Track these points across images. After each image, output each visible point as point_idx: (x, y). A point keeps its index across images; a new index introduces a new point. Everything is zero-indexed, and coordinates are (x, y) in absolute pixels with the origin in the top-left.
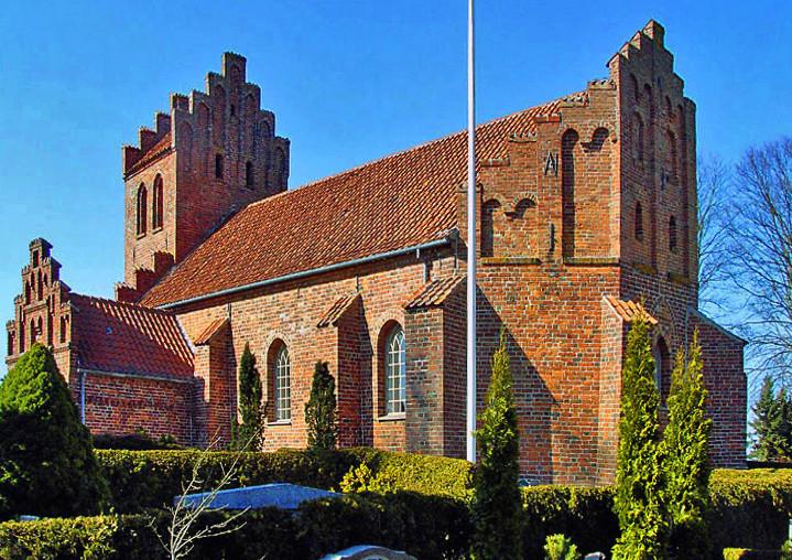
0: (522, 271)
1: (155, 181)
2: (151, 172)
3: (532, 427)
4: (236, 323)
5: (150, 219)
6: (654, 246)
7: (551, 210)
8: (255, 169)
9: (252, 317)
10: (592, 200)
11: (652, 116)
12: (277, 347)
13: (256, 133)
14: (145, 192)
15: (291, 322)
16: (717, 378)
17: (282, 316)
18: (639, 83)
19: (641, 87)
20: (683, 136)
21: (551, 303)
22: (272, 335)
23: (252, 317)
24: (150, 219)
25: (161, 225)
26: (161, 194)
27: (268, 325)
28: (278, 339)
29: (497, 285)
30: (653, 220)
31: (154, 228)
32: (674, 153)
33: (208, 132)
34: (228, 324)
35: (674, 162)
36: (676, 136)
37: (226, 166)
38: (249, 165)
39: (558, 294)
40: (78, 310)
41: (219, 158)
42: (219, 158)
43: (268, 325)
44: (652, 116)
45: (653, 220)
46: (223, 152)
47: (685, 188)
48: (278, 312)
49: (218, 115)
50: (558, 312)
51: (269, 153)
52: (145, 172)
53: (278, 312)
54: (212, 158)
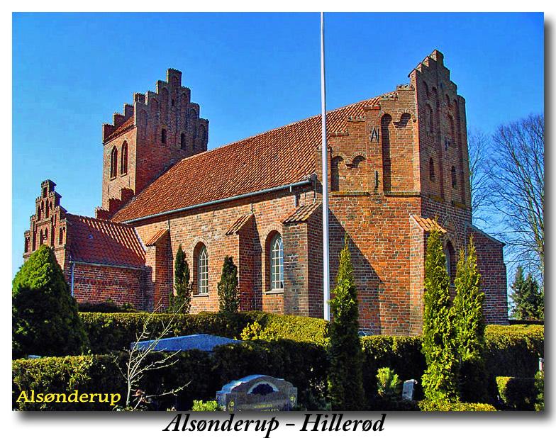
4: (173, 233)
8: (187, 137)
9: (184, 229)
12: (200, 247)
14: (116, 151)
15: (209, 231)
16: (487, 267)
20: (458, 118)
21: (377, 219)
22: (197, 240)
23: (184, 229)
26: (126, 153)
28: (200, 242)
29: (342, 209)
32: (452, 128)
33: (157, 116)
34: (168, 233)
35: (453, 133)
36: (454, 118)
38: (183, 135)
39: (381, 214)
41: (164, 131)
42: (164, 131)
45: (441, 169)
46: (166, 128)
49: (163, 106)
52: (117, 140)
54: (159, 131)
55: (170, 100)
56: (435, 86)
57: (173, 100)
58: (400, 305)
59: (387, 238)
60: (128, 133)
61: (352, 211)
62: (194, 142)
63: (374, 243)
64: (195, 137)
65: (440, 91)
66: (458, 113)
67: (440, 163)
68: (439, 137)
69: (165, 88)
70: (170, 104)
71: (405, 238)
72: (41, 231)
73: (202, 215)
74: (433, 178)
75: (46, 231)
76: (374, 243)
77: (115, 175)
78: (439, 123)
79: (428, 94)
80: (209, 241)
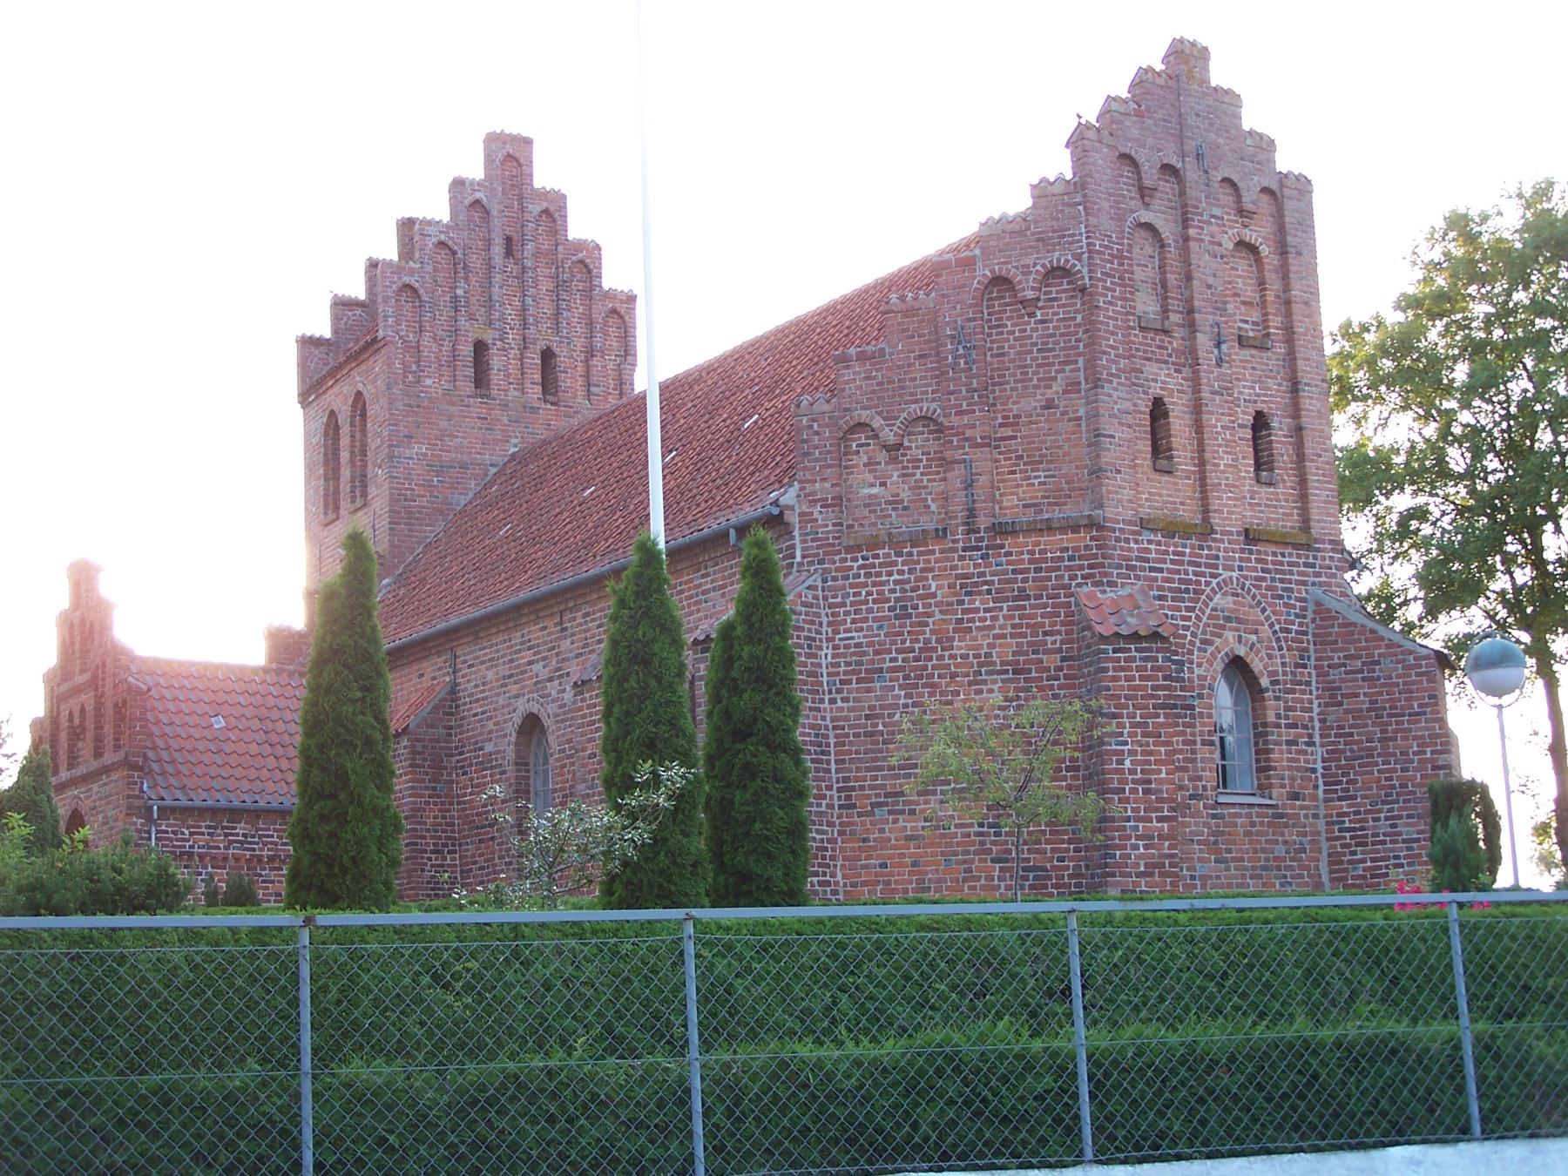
0: (920, 554)
1: (354, 405)
2: (346, 389)
3: (955, 854)
4: (467, 687)
5: (345, 487)
6: (1203, 479)
7: (968, 433)
8: (562, 358)
9: (490, 675)
10: (1047, 407)
11: (1185, 223)
12: (532, 726)
13: (560, 286)
14: (337, 428)
15: (550, 680)
16: (1384, 731)
17: (537, 667)
18: (1145, 167)
19: (1150, 176)
20: (1283, 250)
21: (977, 610)
22: (522, 707)
23: (490, 675)
24: (345, 487)
25: (364, 495)
26: (364, 431)
27: (514, 688)
28: (532, 714)
29: (874, 584)
30: (1199, 427)
31: (353, 501)
32: (1262, 284)
33: (455, 298)
34: (453, 690)
35: (1264, 303)
36: (1265, 250)
37: (496, 361)
38: (547, 355)
39: (989, 592)
40: (777, 639)
41: (480, 348)
42: (480, 348)
43: (514, 688)
44: (1185, 223)
45: (1199, 427)
46: (488, 336)
47: (1291, 355)
48: (530, 663)
49: (475, 261)
50: (992, 627)
51: (590, 324)
52: (336, 389)
53: (530, 663)
54: (466, 350)
55: (498, 241)
56: (1174, 161)
57: (509, 240)
58: (1054, 868)
59: (1008, 663)
60: (363, 367)
61: (904, 591)
62: (587, 375)
63: (970, 684)
64: (590, 353)
65: (1192, 174)
66: (1281, 229)
67: (1197, 409)
68: (1192, 326)
69: (477, 202)
70: (498, 250)
71: (1063, 659)
72: (71, 714)
73: (533, 632)
74: (1162, 463)
75: (83, 710)
76: (970, 684)
77: (337, 509)
78: (1189, 278)
79: (1144, 193)
80: (552, 708)
